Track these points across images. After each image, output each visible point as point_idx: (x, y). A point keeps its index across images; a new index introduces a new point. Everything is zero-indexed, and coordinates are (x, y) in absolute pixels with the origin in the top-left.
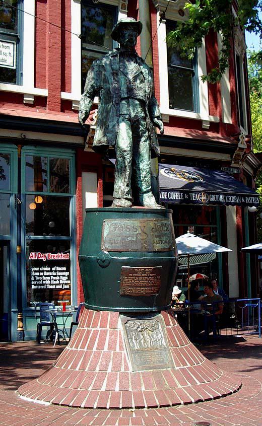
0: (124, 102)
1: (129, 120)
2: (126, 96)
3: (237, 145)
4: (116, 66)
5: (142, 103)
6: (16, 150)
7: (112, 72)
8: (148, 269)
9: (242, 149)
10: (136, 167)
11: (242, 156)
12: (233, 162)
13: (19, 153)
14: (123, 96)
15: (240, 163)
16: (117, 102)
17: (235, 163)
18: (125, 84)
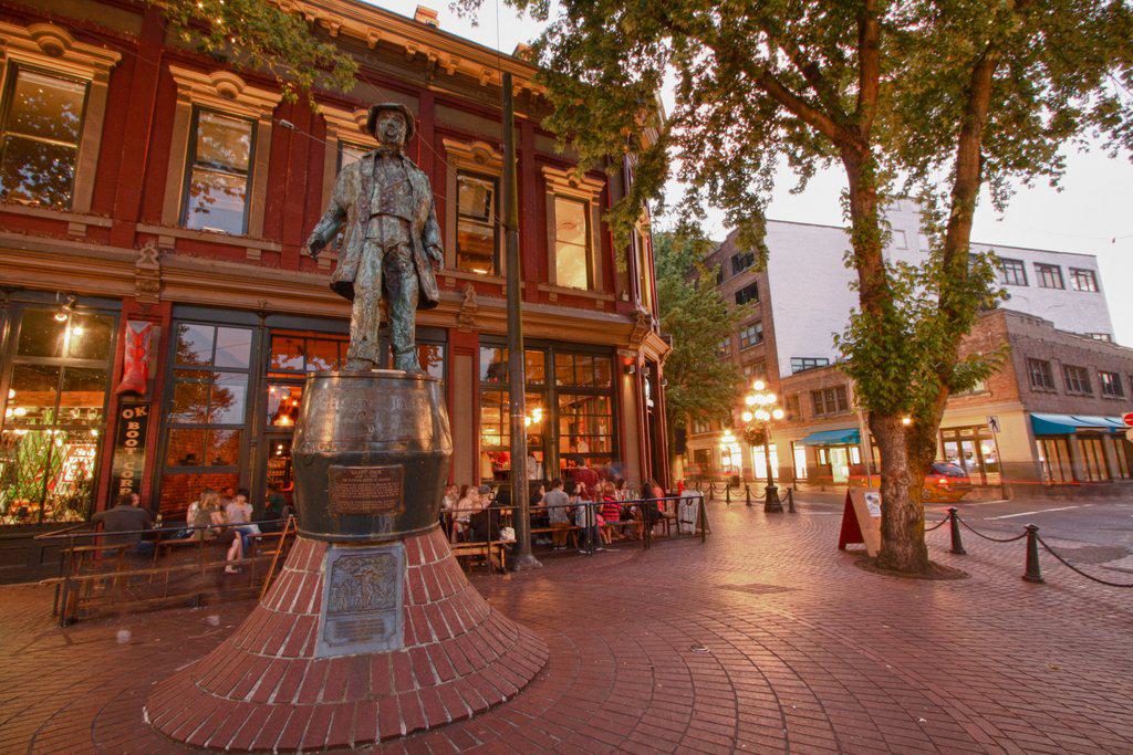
0: (375, 221)
1: (381, 246)
5: (407, 223)
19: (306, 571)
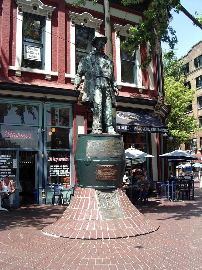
0: (98, 79)
2: (99, 76)
3: (157, 101)
4: (94, 60)
5: (107, 79)
6: (42, 104)
7: (92, 63)
8: (111, 166)
9: (159, 103)
10: (104, 113)
11: (159, 107)
12: (155, 110)
13: (43, 105)
14: (97, 76)
15: (158, 111)
16: (94, 79)
17: (156, 111)
18: (98, 69)
19: (89, 197)
